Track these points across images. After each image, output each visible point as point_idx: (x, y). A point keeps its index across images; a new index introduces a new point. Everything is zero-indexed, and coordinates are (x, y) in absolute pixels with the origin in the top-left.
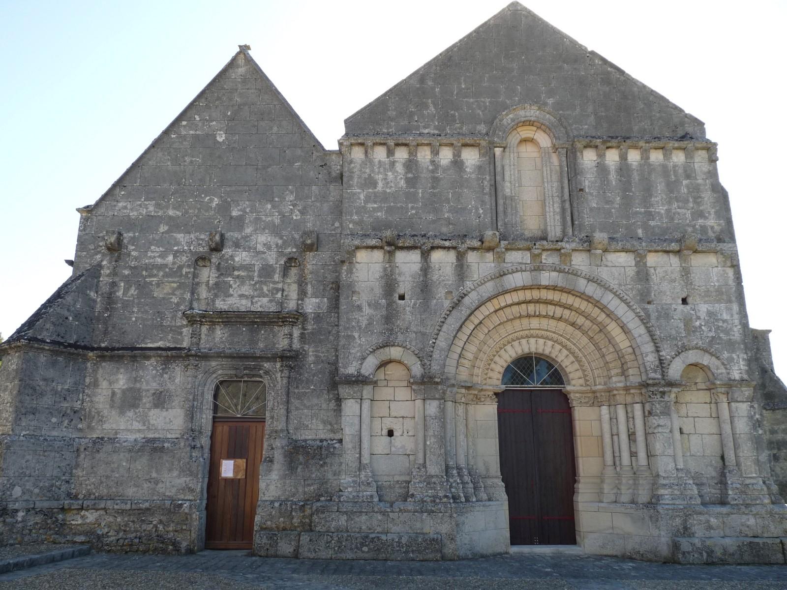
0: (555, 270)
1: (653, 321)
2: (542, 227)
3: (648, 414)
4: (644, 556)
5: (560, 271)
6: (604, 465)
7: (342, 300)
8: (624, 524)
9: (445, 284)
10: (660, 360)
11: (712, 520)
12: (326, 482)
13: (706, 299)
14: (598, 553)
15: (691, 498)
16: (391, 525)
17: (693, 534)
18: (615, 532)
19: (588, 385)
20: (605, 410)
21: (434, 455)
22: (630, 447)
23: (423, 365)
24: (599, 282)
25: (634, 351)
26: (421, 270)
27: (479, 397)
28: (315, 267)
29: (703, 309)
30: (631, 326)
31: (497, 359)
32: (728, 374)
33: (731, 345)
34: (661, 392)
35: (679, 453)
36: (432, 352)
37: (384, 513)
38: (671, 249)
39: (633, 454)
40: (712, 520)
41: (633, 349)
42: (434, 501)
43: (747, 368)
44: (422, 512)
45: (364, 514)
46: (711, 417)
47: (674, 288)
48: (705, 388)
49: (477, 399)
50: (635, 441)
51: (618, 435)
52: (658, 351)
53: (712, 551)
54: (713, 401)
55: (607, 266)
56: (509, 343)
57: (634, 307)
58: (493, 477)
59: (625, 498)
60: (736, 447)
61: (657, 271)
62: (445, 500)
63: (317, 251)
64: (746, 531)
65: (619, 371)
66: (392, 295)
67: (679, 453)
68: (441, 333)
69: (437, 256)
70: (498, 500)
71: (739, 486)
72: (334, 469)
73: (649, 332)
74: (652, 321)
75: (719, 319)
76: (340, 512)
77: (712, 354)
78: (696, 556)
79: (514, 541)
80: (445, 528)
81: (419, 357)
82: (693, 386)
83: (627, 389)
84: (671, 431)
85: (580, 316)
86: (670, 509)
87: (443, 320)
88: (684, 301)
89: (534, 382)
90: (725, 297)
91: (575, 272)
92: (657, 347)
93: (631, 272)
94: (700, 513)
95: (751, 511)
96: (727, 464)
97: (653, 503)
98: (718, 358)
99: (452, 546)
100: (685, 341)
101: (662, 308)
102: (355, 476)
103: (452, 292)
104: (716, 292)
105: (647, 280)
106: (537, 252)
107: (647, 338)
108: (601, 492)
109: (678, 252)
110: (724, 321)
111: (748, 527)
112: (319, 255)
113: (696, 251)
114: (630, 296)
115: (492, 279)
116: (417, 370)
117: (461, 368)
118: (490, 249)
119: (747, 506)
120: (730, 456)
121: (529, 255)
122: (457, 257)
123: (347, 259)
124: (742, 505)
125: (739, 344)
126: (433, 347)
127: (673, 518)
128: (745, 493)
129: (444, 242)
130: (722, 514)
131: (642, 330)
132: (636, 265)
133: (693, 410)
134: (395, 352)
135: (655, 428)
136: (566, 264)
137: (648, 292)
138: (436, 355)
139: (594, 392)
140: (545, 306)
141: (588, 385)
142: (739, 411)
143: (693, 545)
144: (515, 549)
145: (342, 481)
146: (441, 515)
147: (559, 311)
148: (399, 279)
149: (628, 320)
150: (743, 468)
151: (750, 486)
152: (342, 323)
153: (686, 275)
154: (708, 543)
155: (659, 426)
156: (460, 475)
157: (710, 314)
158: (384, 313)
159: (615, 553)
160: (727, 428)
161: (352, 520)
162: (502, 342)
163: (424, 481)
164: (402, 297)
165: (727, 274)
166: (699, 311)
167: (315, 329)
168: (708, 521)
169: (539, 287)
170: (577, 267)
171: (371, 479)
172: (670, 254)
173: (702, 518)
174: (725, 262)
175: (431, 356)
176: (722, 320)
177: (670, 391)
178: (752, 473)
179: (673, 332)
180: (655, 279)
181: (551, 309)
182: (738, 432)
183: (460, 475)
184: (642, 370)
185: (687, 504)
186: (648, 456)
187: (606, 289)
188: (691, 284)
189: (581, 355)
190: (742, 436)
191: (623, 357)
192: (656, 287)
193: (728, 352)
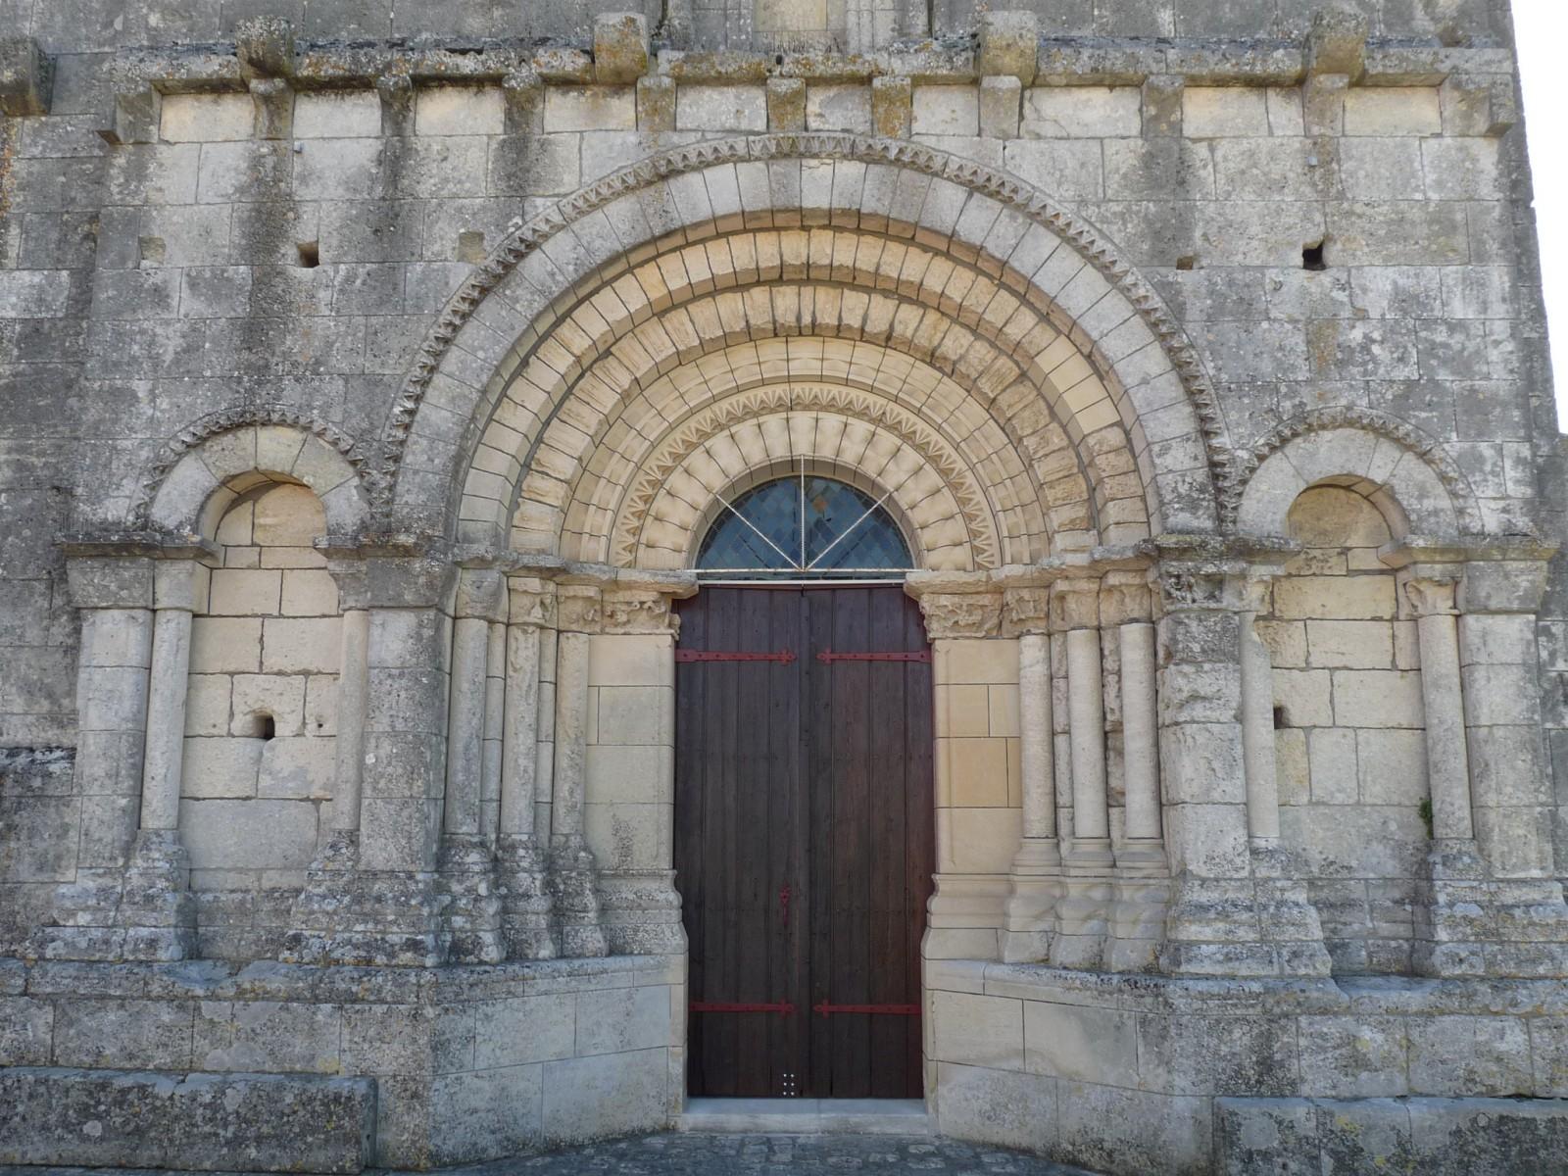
0: (852, 155)
1: (1194, 329)
2: (835, 24)
3: (1161, 658)
4: (1117, 1156)
5: (870, 158)
6: (1022, 835)
7: (105, 272)
8: (1061, 1042)
9: (460, 210)
10: (1213, 465)
11: (1366, 1034)
13: (1394, 248)
14: (976, 1136)
15: (1295, 955)
16: (203, 1044)
17: (1293, 1083)
18: (1030, 1069)
19: (979, 566)
20: (1032, 648)
21: (388, 800)
22: (1107, 774)
23: (368, 489)
24: (1006, 192)
25: (1129, 440)
26: (380, 163)
27: (609, 610)
28: (36, 167)
29: (1379, 283)
30: (1113, 347)
31: (677, 480)
32: (1461, 512)
33: (1475, 411)
34: (1208, 577)
35: (1267, 796)
36: (402, 443)
37: (183, 1003)
38: (1272, 69)
39: (1112, 799)
40: (1366, 1034)
41: (1127, 433)
42: (369, 962)
43: (1529, 492)
44: (316, 1000)
45: (113, 1004)
46: (1394, 667)
47: (1279, 211)
48: (1377, 565)
49: (603, 616)
50: (1121, 753)
51: (1067, 732)
52: (1206, 434)
53: (1357, 1151)
55: (1038, 137)
56: (720, 427)
57: (1129, 280)
58: (641, 875)
59: (1069, 952)
60: (1476, 771)
61: (1219, 155)
62: (407, 957)
63: (47, 112)
64: (1489, 1074)
65: (1081, 512)
66: (272, 251)
67: (1267, 796)
68: (438, 379)
69: (437, 112)
70: (649, 953)
71: (1475, 912)
72: (40, 846)
73: (1179, 366)
75: (1435, 321)
76: (34, 996)
77: (1403, 444)
78: (1293, 1166)
79: (702, 1081)
80: (389, 1058)
81: (354, 463)
82: (1334, 560)
83: (1098, 571)
84: (1240, 718)
85: (957, 328)
86: (1212, 996)
87: (443, 332)
88: (1314, 258)
89: (796, 556)
90: (1460, 241)
91: (922, 160)
92: (1203, 419)
93: (1125, 156)
94: (1324, 1011)
95: (1514, 1004)
96: (1439, 832)
97: (1155, 974)
98: (1424, 456)
99: (411, 1121)
100: (1307, 396)
101: (1231, 283)
102: (108, 872)
103: (481, 236)
104: (1430, 223)
105: (1182, 183)
106: (784, 86)
107: (1169, 387)
108: (999, 931)
109: (1298, 84)
110: (1454, 327)
111: (1499, 1060)
112: (55, 125)
113: (1361, 81)
114: (1115, 238)
115: (629, 189)
116: (347, 506)
117: (528, 508)
118: (622, 83)
119: (1501, 983)
120: (1452, 806)
121: (761, 101)
122: (509, 114)
123: (125, 131)
124: (1482, 979)
125: (1505, 405)
126: (407, 427)
127: (1220, 1027)
128: (1495, 936)
129: (459, 59)
130: (1405, 1014)
131: (1155, 360)
132: (1143, 134)
133: (1330, 643)
134: (273, 448)
135: (1181, 706)
136: (891, 133)
137: (1184, 228)
138: (416, 455)
139: (999, 590)
140: (833, 293)
141: (979, 566)
142: (1492, 646)
143: (1284, 1126)
144: (702, 1116)
145: (63, 889)
146: (379, 1009)
147: (882, 312)
148: (302, 193)
149: (1105, 326)
150: (1496, 846)
151: (1517, 912)
152: (97, 349)
153: (1325, 164)
154: (1343, 1119)
155: (1195, 697)
156: (498, 867)
157: (1404, 301)
158: (242, 308)
159: (1025, 1141)
160: (1446, 705)
161: (71, 1024)
163: (346, 892)
164: (310, 258)
165: (1475, 160)
166: (1365, 290)
168: (1351, 1040)
169: (803, 220)
170: (931, 142)
171: (161, 884)
172: (1271, 93)
173: (1330, 1027)
174: (1467, 116)
175: (397, 459)
176: (1445, 322)
177: (1243, 576)
178: (1526, 864)
179: (1266, 366)
180: (1208, 178)
181: (853, 306)
182: (1484, 720)
183: (498, 867)
184: (1152, 502)
185: (1281, 977)
186: (1161, 805)
187: (1034, 217)
188: (1341, 196)
189: (960, 465)
190: (1499, 733)
191: (1091, 464)
193: (1464, 436)
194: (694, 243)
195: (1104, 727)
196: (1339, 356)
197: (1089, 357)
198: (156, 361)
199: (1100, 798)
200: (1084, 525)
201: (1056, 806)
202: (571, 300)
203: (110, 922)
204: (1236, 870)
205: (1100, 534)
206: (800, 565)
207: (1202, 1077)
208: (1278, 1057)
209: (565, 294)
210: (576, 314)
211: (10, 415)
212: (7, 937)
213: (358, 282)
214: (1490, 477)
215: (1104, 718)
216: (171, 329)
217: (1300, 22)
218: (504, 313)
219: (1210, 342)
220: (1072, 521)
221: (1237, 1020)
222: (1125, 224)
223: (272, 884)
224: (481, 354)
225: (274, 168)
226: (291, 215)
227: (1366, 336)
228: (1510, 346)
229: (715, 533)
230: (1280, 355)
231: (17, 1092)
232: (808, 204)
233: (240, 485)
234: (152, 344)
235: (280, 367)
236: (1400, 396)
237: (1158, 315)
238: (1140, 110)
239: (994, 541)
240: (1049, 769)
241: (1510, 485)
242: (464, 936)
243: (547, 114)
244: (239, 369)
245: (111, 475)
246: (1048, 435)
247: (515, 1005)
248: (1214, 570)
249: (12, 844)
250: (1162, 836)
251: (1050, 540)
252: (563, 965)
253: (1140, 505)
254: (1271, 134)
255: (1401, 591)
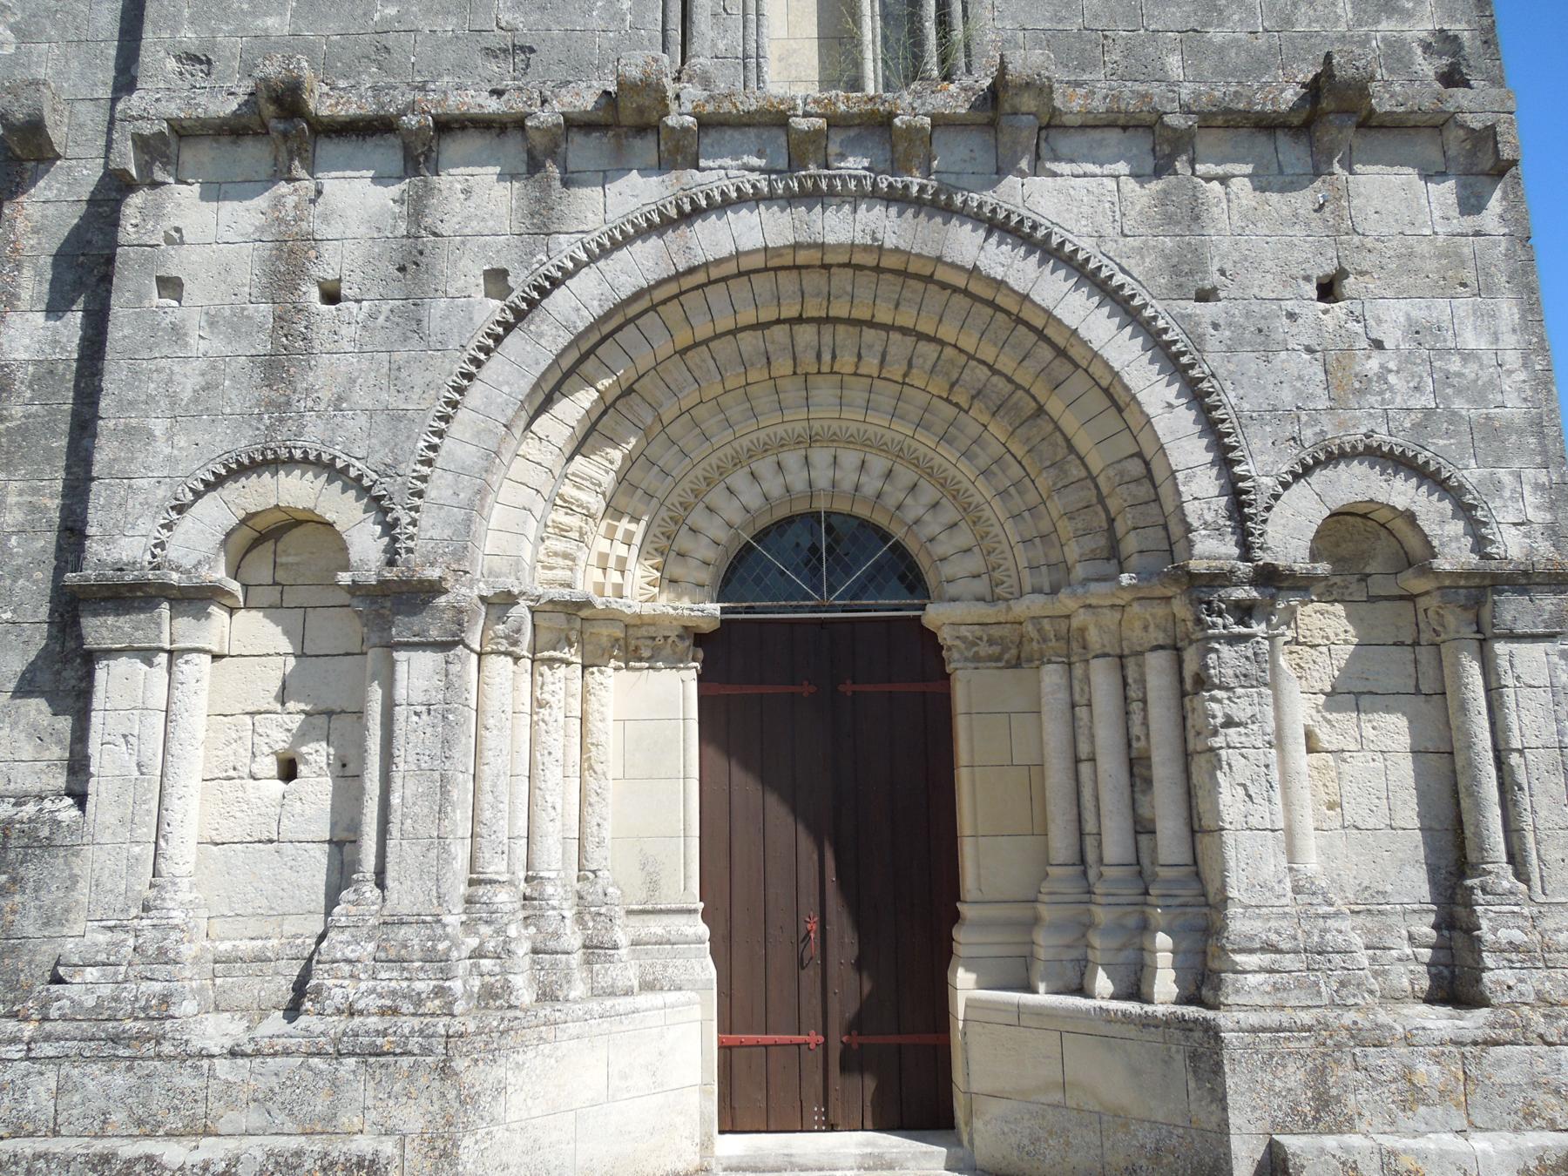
9: (484, 247)
12: (14, 948)
13: (1405, 280)
20: (1051, 677)
22: (1134, 801)
39: (1142, 828)
46: (1418, 692)
50: (1148, 782)
51: (1093, 759)
54: (1426, 637)
65: (1102, 541)
68: (462, 415)
74: (1209, 357)
82: (1354, 587)
89: (817, 589)
100: (1328, 425)
105: (1197, 218)
110: (1468, 356)
125: (1520, 432)
146: (405, 1062)
157: (1416, 331)
162: (713, 460)
166: (1379, 321)
167: (36, 416)
168: (1407, 1073)
172: (1279, 133)
179: (1287, 397)
186: (1193, 832)
192: (1226, 244)
194: (716, 281)
195: (1129, 754)
196: (1357, 385)
197: (1106, 391)
198: (173, 400)
199: (1127, 824)
200: (1105, 554)
201: (1081, 834)
202: (595, 337)
203: (120, 978)
204: (1278, 897)
205: (1120, 563)
206: (822, 596)
207: (1258, 1114)
208: (1334, 1092)
209: (589, 329)
210: (599, 351)
211: (23, 456)
212: (10, 996)
213: (381, 319)
214: (1509, 503)
215: (1129, 745)
216: (188, 367)
217: (1303, 66)
218: (528, 348)
219: (1231, 373)
220: (1092, 551)
221: (1289, 1054)
222: (1142, 257)
223: (294, 931)
224: (506, 389)
225: (295, 207)
226: (312, 254)
227: (1382, 366)
228: (1522, 375)
229: (735, 568)
230: (1298, 384)
231: (13, 1168)
232: (830, 239)
233: (261, 524)
234: (169, 381)
235: (302, 403)
236: (1419, 424)
237: (1179, 345)
238: (1153, 150)
239: (1013, 573)
240: (1074, 796)
241: (1530, 510)
242: (492, 980)
243: (570, 155)
244: (259, 406)
245: (126, 515)
246: (1067, 467)
247: (547, 1052)
248: (1244, 595)
249: (17, 898)
250: (1195, 862)
251: (1069, 570)
252: (594, 1006)
253: (1162, 534)
254: (1281, 172)
255: (1421, 616)
